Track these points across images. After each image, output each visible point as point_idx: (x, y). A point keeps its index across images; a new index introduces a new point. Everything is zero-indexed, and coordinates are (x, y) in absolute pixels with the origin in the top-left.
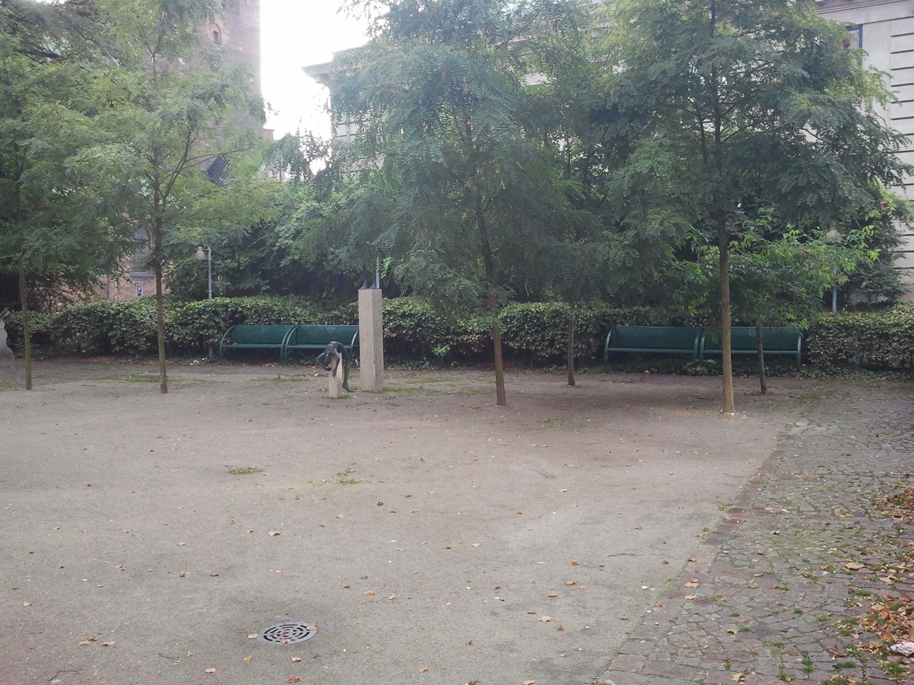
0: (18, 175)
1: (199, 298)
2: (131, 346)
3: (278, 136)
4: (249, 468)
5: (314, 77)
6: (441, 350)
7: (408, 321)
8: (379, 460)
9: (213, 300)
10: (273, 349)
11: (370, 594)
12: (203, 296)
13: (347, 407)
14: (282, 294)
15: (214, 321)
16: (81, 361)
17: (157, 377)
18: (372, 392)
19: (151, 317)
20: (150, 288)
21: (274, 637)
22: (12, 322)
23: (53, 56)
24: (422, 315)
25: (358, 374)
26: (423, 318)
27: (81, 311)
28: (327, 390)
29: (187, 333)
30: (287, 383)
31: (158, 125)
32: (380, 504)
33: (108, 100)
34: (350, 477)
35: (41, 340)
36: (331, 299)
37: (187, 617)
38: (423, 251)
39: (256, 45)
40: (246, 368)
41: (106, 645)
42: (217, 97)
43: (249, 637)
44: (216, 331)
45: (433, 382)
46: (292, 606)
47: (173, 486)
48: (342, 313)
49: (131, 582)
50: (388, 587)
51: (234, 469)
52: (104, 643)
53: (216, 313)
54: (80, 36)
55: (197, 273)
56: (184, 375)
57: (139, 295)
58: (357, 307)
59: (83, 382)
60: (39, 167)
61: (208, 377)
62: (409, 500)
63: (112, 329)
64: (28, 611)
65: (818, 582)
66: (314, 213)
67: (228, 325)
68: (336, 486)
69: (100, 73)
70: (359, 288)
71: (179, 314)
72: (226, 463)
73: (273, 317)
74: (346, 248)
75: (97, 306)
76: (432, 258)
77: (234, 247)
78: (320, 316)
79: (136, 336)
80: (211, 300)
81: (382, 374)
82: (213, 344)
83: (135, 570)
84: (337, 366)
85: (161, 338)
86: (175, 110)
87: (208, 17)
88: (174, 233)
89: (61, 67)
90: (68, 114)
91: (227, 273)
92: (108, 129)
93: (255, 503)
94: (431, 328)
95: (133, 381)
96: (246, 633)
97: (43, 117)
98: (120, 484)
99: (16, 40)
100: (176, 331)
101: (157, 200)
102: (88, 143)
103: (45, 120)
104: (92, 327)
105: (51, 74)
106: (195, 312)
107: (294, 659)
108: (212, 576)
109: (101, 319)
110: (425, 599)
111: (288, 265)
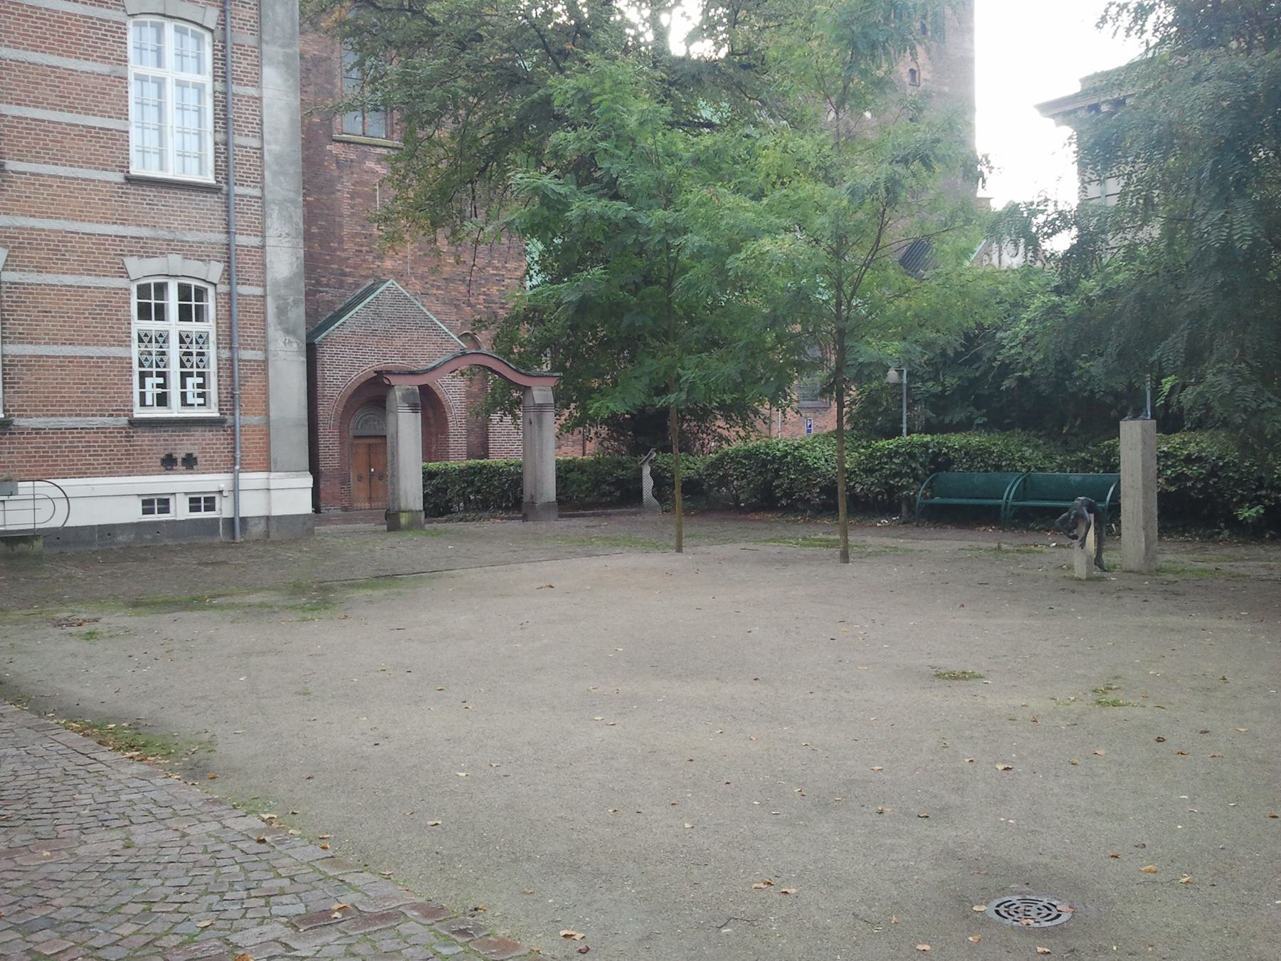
0: (670, 280)
1: (889, 436)
2: (801, 499)
3: (998, 205)
4: (964, 673)
5: (1053, 116)
6: (1248, 513)
7: (1195, 468)
8: (1154, 675)
9: (908, 438)
10: (990, 507)
11: (1150, 871)
12: (895, 432)
13: (1102, 593)
14: (1004, 428)
15: (910, 467)
16: (740, 517)
17: (834, 540)
18: (1137, 572)
19: (826, 460)
20: (828, 422)
21: (1009, 914)
22: (659, 467)
23: (709, 125)
24: (1218, 458)
25: (1117, 546)
26: (1221, 464)
27: (741, 453)
28: (1070, 568)
29: (873, 483)
30: (1011, 554)
31: (845, 203)
32: (1160, 740)
33: (779, 177)
34: (1111, 697)
35: (693, 488)
36: (1076, 435)
37: (888, 869)
38: (1226, 365)
39: (968, 80)
40: (951, 532)
41: (786, 892)
42: (924, 158)
43: (974, 908)
44: (911, 481)
45: (1236, 560)
46: (1034, 873)
47: (863, 689)
48: (1091, 456)
49: (814, 812)
50: (1178, 864)
51: (943, 672)
52: (784, 890)
53: (912, 456)
54: (743, 95)
55: (887, 400)
56: (869, 540)
57: (809, 431)
58: (1116, 446)
59: (743, 545)
60: (699, 270)
61: (901, 543)
62: (1206, 737)
63: (778, 476)
64: (691, 835)
65: (121, 842)
66: (1053, 310)
67: (928, 473)
68: (1091, 707)
69: (768, 140)
70: (1122, 416)
71: (863, 458)
72: (931, 662)
73: (990, 462)
74: (1102, 360)
75: (759, 446)
76: (1242, 376)
77: (942, 362)
78: (1059, 459)
79: (808, 485)
80: (906, 438)
81: (1156, 546)
82: (907, 498)
83: (818, 797)
84: (1086, 534)
85: (841, 488)
86: (868, 181)
87: (908, 51)
88: (863, 348)
89: (719, 137)
90: (731, 200)
91: (926, 401)
92: (779, 215)
93: (974, 722)
94: (1232, 478)
95: (805, 546)
96: (971, 902)
97: (701, 207)
98: (795, 680)
99: (666, 110)
100: (858, 479)
101: (839, 304)
102: (755, 235)
103: (703, 210)
104: (754, 474)
105: (707, 148)
106: (884, 454)
107: (1040, 949)
108: (919, 816)
109: (764, 463)
110: (1238, 890)
111: (1014, 388)
